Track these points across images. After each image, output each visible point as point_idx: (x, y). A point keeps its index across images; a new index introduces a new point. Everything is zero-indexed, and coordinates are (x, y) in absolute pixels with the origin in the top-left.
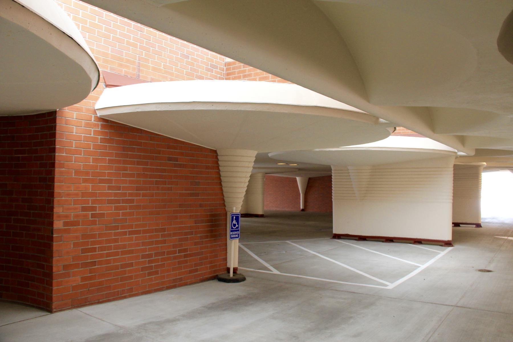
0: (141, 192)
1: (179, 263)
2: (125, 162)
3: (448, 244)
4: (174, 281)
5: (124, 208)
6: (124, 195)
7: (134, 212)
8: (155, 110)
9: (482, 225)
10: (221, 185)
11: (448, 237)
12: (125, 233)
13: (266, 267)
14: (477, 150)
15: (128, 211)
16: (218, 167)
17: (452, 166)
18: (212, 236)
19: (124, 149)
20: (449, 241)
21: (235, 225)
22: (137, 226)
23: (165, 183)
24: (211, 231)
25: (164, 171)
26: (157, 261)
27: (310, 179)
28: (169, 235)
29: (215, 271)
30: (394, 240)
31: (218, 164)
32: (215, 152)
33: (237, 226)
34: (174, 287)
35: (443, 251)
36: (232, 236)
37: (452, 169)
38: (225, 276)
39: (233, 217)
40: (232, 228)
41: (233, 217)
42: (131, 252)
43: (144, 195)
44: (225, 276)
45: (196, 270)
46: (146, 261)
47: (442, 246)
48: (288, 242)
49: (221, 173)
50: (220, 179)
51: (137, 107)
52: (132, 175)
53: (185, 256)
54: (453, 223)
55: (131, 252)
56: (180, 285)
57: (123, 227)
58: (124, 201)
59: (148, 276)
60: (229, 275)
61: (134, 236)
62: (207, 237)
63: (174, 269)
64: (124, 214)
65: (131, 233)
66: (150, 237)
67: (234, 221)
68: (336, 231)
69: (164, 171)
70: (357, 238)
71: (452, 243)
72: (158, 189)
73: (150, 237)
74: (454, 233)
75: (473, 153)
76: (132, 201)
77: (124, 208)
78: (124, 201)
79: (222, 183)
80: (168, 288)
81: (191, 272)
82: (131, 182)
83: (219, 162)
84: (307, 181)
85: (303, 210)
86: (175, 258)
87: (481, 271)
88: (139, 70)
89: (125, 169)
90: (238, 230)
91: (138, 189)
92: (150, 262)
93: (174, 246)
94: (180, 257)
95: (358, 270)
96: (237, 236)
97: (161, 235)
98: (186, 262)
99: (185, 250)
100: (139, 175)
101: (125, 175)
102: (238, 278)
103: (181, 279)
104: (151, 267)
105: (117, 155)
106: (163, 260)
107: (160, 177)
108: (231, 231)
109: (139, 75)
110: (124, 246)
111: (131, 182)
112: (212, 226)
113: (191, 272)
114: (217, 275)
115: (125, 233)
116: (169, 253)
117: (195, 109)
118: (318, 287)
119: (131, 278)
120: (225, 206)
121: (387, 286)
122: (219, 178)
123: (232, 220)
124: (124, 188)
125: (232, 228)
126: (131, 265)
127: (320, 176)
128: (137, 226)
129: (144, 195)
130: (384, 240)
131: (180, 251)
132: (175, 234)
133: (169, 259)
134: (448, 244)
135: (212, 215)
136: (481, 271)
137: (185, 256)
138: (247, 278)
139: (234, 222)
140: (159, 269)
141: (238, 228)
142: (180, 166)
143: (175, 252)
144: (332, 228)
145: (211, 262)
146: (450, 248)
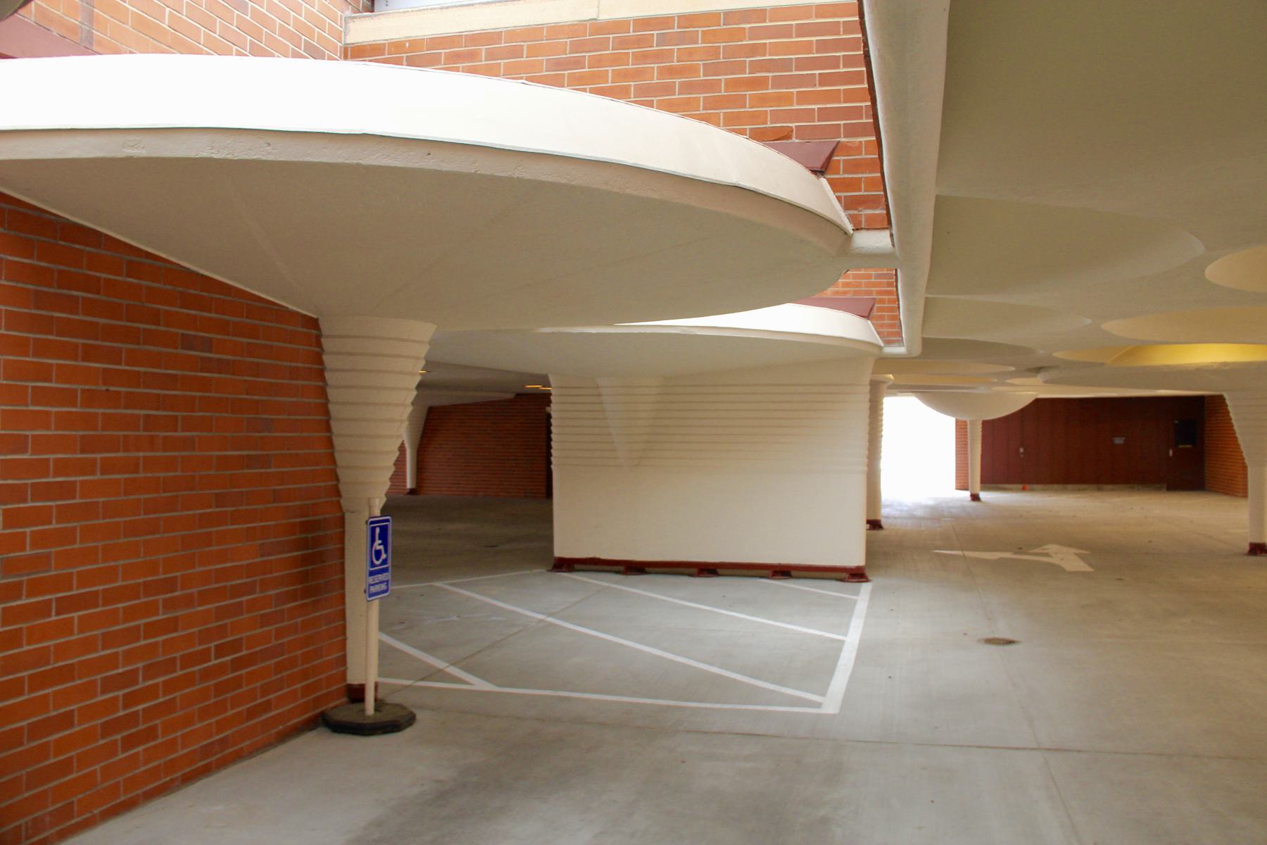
0: (98, 456)
1: (220, 689)
2: (43, 349)
3: (857, 575)
4: (206, 751)
5: (42, 516)
6: (40, 467)
7: (75, 528)
8: (205, 154)
9: (883, 522)
10: (328, 428)
11: (856, 558)
12: (43, 609)
13: (440, 671)
14: (926, 342)
15: (54, 525)
16: (321, 374)
17: (868, 382)
18: (306, 593)
19: (40, 300)
20: (859, 568)
21: (378, 554)
22: (85, 579)
23: (172, 424)
24: (303, 577)
25: (171, 381)
26: (150, 692)
27: (431, 410)
28: (188, 601)
29: (317, 701)
30: (719, 571)
31: (321, 362)
32: (313, 323)
33: (384, 556)
34: (206, 771)
35: (857, 593)
36: (373, 589)
37: (868, 388)
38: (348, 714)
39: (373, 530)
40: (373, 565)
41: (373, 530)
42: (65, 674)
43: (108, 467)
44: (350, 715)
45: (267, 706)
46: (116, 698)
47: (842, 580)
48: (438, 584)
49: (330, 392)
50: (327, 413)
51: (132, 138)
52: (67, 397)
53: (237, 664)
54: (868, 522)
55: (65, 674)
56: (223, 763)
57: (36, 587)
58: (43, 492)
59: (124, 750)
60: (363, 710)
61: (76, 615)
62: (293, 596)
63: (205, 713)
64: (39, 539)
65: (66, 605)
66: (130, 614)
67: (378, 541)
68: (562, 549)
69: (171, 381)
70: (622, 568)
71: (868, 573)
72: (151, 444)
73: (130, 614)
74: (870, 552)
75: (917, 350)
76: (65, 490)
77: (42, 516)
78: (43, 492)
79: (333, 423)
80: (188, 779)
81: (252, 713)
82: (65, 421)
83: (325, 358)
84: (424, 416)
85: (412, 492)
86: (206, 674)
87: (990, 641)
88: (91, 17)
89: (43, 373)
90: (386, 570)
91: (88, 445)
92: (130, 700)
93: (205, 636)
94: (221, 669)
95: (674, 653)
96: (383, 587)
97: (165, 601)
98: (237, 683)
99: (236, 646)
100: (91, 398)
101: (41, 396)
102: (393, 722)
103: (223, 743)
104: (132, 719)
105: (14, 321)
106: (170, 686)
107: (160, 402)
108: (372, 574)
109: (90, 33)
110: (41, 657)
111: (65, 421)
112: (306, 560)
113: (252, 713)
114: (322, 714)
115: (43, 609)
116: (188, 661)
117: (364, 162)
118: (645, 728)
119: (65, 767)
120: (338, 493)
121: (819, 705)
122: (324, 409)
123: (373, 540)
124: (41, 444)
125: (373, 565)
126: (66, 720)
127: (459, 402)
128: (85, 579)
129: (108, 467)
130: (694, 570)
131: (220, 651)
132: (204, 597)
133: (189, 680)
134: (857, 575)
135: (306, 527)
136: (990, 641)
137: (237, 664)
138: (420, 715)
139: (378, 545)
140: (157, 722)
141: (385, 561)
142: (221, 366)
143: (204, 656)
144: (550, 539)
145: (305, 675)
146: (866, 588)
